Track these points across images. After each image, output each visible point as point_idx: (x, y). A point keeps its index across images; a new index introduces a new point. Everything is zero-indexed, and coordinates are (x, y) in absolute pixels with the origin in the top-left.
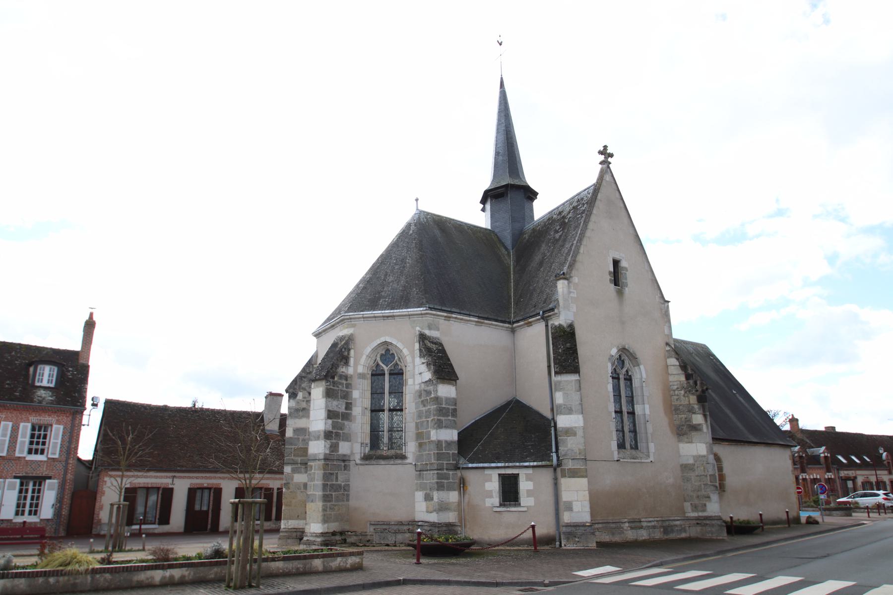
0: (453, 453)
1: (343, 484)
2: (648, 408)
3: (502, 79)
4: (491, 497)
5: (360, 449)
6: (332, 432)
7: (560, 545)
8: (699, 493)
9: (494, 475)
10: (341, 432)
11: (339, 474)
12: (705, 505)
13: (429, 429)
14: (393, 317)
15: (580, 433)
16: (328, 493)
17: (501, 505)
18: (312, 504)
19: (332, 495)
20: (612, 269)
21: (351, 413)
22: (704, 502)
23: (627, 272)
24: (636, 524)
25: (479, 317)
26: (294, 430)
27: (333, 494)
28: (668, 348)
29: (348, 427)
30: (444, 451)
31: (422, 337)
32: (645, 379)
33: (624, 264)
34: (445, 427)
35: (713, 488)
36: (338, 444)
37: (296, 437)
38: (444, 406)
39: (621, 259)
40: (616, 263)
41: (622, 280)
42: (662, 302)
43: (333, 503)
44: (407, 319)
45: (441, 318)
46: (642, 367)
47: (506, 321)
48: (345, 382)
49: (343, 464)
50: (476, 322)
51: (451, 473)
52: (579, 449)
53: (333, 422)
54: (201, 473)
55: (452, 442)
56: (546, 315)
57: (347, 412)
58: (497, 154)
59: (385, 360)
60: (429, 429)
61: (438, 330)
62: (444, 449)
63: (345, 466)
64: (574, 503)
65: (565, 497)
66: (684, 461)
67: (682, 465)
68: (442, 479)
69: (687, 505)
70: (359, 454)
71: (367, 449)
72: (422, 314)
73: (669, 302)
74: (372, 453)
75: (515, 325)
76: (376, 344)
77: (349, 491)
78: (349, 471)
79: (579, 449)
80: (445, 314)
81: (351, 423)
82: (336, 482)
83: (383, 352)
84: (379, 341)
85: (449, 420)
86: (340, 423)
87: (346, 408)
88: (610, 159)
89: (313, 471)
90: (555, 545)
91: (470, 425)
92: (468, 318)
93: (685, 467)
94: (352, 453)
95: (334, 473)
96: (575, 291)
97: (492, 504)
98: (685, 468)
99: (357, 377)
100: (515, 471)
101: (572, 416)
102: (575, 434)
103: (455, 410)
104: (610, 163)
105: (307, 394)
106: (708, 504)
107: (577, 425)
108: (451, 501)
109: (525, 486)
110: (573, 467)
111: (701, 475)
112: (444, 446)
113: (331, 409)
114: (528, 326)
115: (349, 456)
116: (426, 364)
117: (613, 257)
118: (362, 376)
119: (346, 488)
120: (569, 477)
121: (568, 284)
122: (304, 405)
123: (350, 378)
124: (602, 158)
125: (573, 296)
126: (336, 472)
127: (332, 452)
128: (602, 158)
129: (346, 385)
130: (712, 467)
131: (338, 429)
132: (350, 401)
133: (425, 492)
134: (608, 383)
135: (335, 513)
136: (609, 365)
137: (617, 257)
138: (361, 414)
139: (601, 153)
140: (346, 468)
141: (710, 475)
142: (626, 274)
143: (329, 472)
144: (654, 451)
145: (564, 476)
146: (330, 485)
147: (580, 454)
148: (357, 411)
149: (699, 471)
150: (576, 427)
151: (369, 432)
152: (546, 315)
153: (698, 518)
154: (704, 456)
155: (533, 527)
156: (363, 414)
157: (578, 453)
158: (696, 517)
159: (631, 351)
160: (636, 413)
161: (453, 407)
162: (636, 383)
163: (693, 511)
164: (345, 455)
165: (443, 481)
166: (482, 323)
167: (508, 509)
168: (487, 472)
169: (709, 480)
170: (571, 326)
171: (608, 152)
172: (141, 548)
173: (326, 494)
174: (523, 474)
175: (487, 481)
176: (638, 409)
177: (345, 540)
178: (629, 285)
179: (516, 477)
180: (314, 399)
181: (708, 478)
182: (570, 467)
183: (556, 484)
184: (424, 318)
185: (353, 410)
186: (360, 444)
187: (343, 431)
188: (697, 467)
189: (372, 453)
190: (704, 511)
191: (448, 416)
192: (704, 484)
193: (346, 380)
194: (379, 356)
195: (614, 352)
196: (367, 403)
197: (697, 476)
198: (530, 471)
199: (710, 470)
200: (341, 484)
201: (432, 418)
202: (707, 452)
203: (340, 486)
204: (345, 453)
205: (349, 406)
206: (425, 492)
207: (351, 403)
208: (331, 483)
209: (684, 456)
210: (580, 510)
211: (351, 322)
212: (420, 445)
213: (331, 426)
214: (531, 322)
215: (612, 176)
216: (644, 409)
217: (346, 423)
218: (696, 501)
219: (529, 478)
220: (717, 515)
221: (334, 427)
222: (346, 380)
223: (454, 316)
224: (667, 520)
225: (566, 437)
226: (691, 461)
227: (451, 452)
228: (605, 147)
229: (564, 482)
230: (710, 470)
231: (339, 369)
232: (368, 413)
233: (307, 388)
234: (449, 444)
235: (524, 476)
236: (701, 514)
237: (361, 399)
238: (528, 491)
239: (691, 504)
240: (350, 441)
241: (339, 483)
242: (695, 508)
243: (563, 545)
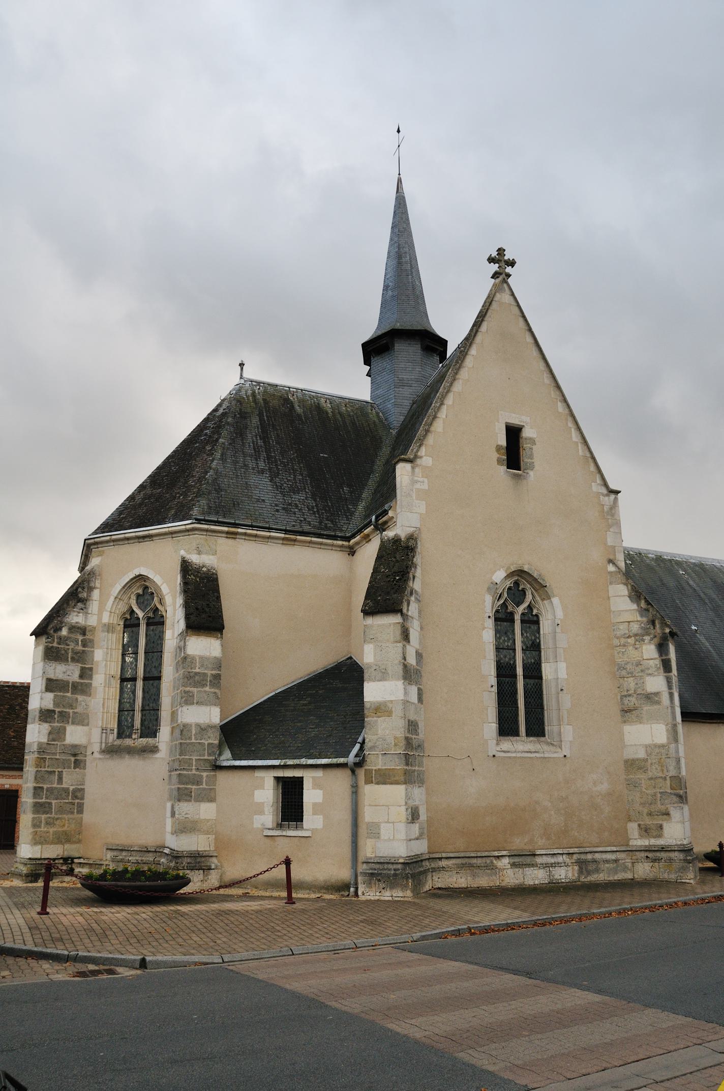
0: (209, 744)
1: (71, 788)
2: (565, 668)
3: (400, 181)
4: (262, 812)
5: (99, 737)
6: (54, 711)
7: (356, 895)
8: (653, 808)
9: (268, 779)
10: (71, 711)
11: (64, 773)
12: (661, 827)
14: (150, 537)
15: (398, 711)
16: (43, 800)
17: (280, 826)
19: (50, 804)
20: (503, 442)
21: (91, 683)
22: (660, 822)
23: (534, 447)
24: (524, 858)
25: (286, 531)
27: (54, 802)
28: (611, 568)
29: (83, 704)
30: (193, 741)
31: (186, 567)
32: (561, 620)
33: (527, 433)
34: (197, 703)
35: (675, 799)
36: (65, 729)
38: (197, 670)
39: (523, 426)
40: (513, 433)
41: (524, 459)
42: (604, 491)
43: (53, 815)
45: (219, 535)
46: (556, 601)
47: (338, 537)
48: (80, 638)
49: (73, 759)
51: (205, 774)
52: (395, 738)
53: (55, 696)
54: (6, 770)
55: (212, 727)
56: (380, 522)
57: (82, 681)
58: (386, 288)
59: (143, 603)
61: (215, 553)
62: (193, 737)
63: (76, 761)
64: (382, 825)
65: (368, 815)
66: (630, 754)
67: (626, 761)
68: (187, 783)
69: (633, 828)
70: (98, 745)
71: (112, 737)
72: (188, 530)
73: (617, 492)
74: (118, 742)
75: (353, 541)
76: (131, 577)
77: (82, 798)
78: (84, 768)
79: (395, 738)
80: (226, 529)
81: (90, 698)
82: (58, 783)
83: (140, 591)
84: (131, 575)
85: (205, 692)
86: (69, 697)
87: (81, 676)
88: (509, 270)
90: (349, 891)
91: (265, 701)
92: (268, 534)
93: (632, 764)
94: (89, 742)
95: (55, 772)
96: (426, 480)
97: (263, 825)
98: (632, 765)
99: (101, 629)
100: (297, 773)
101: (386, 683)
102: (389, 713)
103: (217, 677)
104: (509, 275)
106: (665, 825)
107: (393, 698)
108: (202, 817)
109: (311, 796)
110: (384, 768)
111: (656, 778)
112: (194, 732)
113: (52, 676)
114: (367, 542)
115: (86, 747)
117: (506, 423)
118: (109, 628)
119: (79, 795)
120: (378, 783)
121: (413, 468)
123: (91, 631)
124: (495, 267)
125: (423, 487)
126: (60, 770)
127: (54, 740)
128: (495, 267)
129: (82, 641)
130: (674, 764)
131: (64, 706)
132: (90, 666)
134: (484, 628)
135: (55, 829)
136: (489, 599)
137: (515, 420)
138: (103, 685)
139: (491, 260)
140: (78, 764)
141: (670, 777)
142: (531, 449)
143: (46, 769)
144: (571, 739)
145: (369, 781)
146: (48, 789)
147: (396, 745)
148: (98, 680)
149: (654, 771)
150: (391, 701)
151: (117, 712)
152: (380, 522)
153: (648, 850)
154: (663, 746)
155: (288, 862)
156: (108, 685)
157: (393, 744)
158: (646, 846)
159: (535, 575)
160: (544, 678)
161: (214, 672)
162: (546, 626)
163: (641, 836)
164: (75, 746)
165: (189, 786)
166: (295, 540)
167: (284, 833)
168: (259, 774)
169: (669, 784)
170: (411, 537)
171: (506, 258)
173: (39, 803)
174: (309, 778)
175: (257, 788)
176: (547, 670)
177: (72, 870)
178: (537, 467)
179: (299, 782)
181: (668, 782)
182: (380, 767)
183: (355, 791)
184: (191, 536)
185: (94, 678)
186: (100, 730)
187: (75, 711)
188: (652, 764)
189: (118, 742)
190: (660, 836)
191: (204, 685)
192: (661, 793)
193: (84, 634)
194: (134, 597)
195: (499, 576)
196: (115, 669)
197: (651, 779)
198: (319, 773)
199: (671, 768)
200: (69, 788)
202: (668, 738)
203: (66, 790)
204: (77, 742)
205: (86, 673)
207: (91, 669)
208: (49, 786)
209: (631, 745)
210: (392, 838)
211: (98, 548)
213: (52, 702)
215: (513, 294)
216: (556, 671)
217: (80, 698)
218: (648, 821)
219: (316, 785)
220: (679, 843)
221: (56, 704)
222: (84, 634)
223: (240, 530)
224: (591, 852)
225: (375, 719)
226: (642, 754)
227: (206, 743)
228: (501, 251)
229: (371, 792)
230: (671, 768)
231: (71, 616)
232: (116, 684)
234: (203, 729)
235: (311, 780)
236: (653, 841)
237: (105, 662)
238: (315, 804)
239: (639, 825)
240: (88, 725)
241: (64, 786)
242: (645, 831)
243: (360, 893)
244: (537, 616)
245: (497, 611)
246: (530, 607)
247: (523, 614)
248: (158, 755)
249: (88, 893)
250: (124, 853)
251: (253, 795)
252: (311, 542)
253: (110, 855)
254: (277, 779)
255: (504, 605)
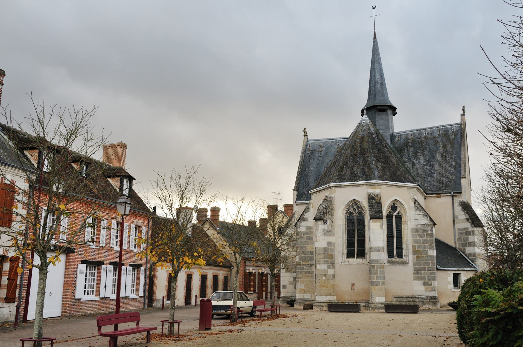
3: (374, 32)
4: (450, 284)
9: (451, 274)
13: (427, 249)
18: (376, 286)
26: (327, 243)
37: (328, 247)
44: (406, 188)
50: (437, 196)
60: (427, 249)
89: (376, 269)
105: (331, 222)
116: (422, 215)
122: (330, 228)
133: (423, 281)
168: (449, 272)
172: (279, 307)
180: (373, 229)
198: (465, 272)
201: (429, 244)
206: (423, 281)
212: (418, 257)
214: (440, 196)
233: (331, 218)
244: (401, 216)
245: (387, 214)
246: (399, 213)
247: (396, 215)
248: (409, 265)
249: (451, 308)
250: (400, 299)
251: (447, 278)
252: (447, 196)
253: (395, 300)
254: (454, 274)
255: (390, 212)
